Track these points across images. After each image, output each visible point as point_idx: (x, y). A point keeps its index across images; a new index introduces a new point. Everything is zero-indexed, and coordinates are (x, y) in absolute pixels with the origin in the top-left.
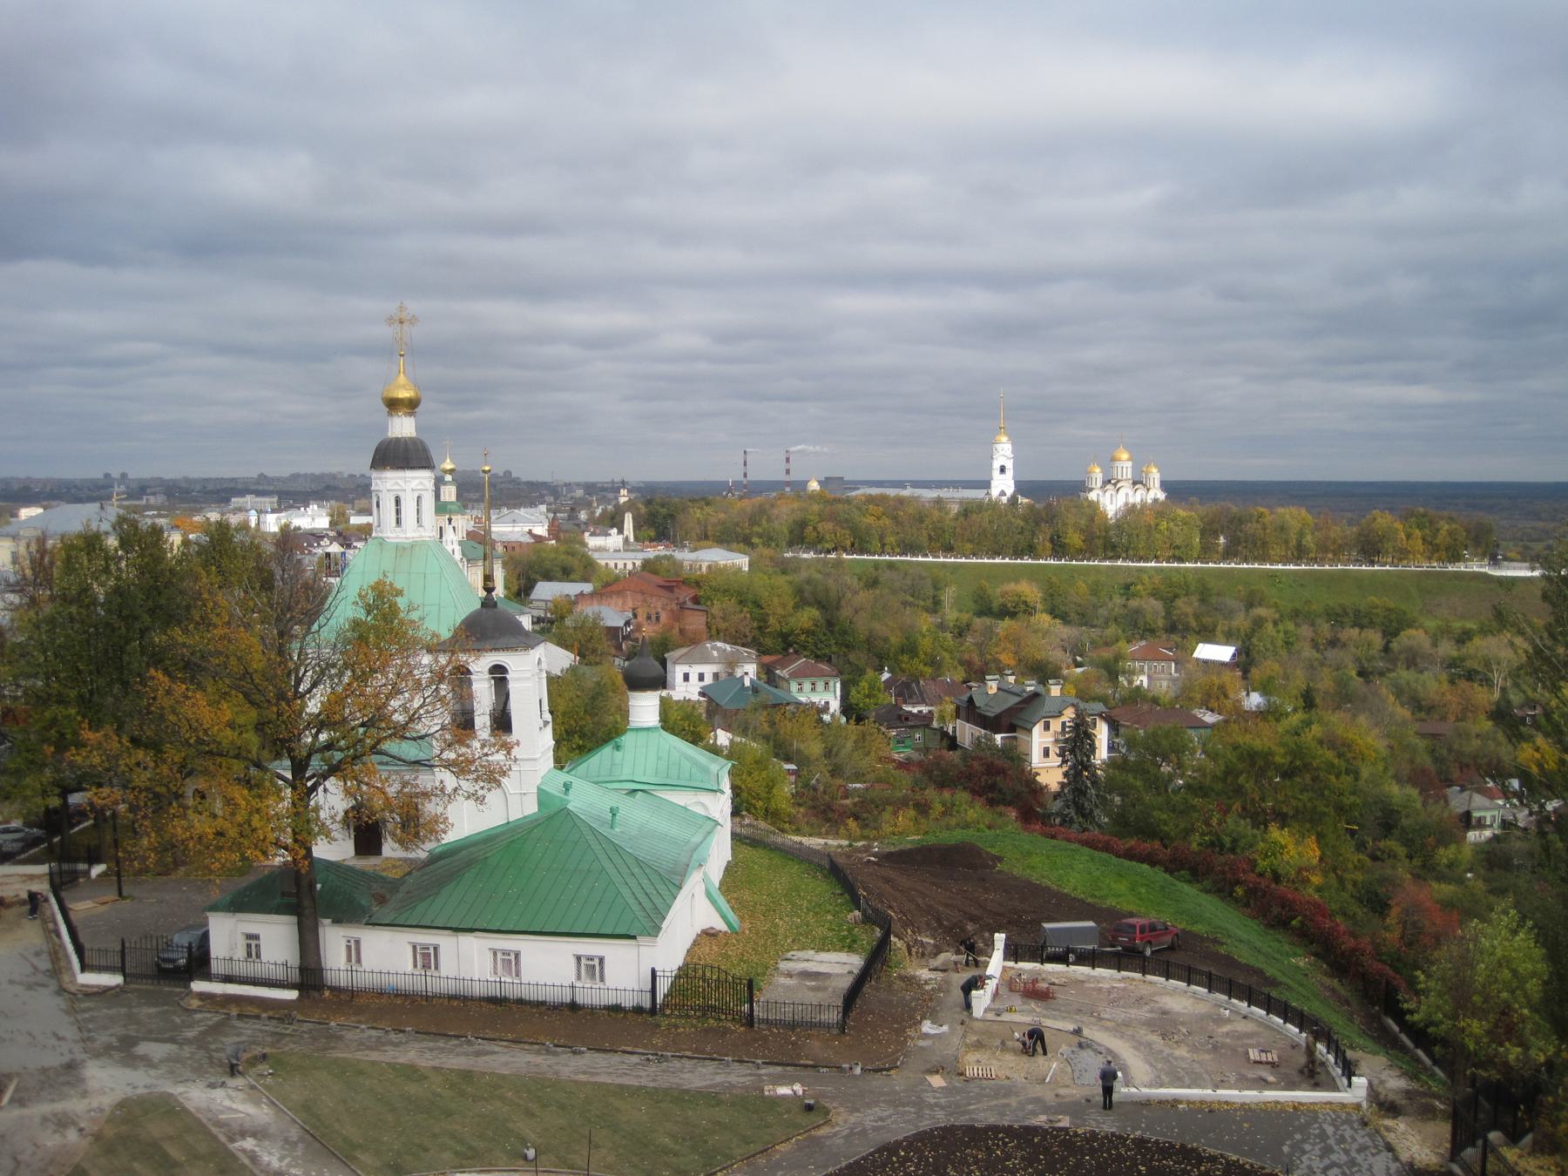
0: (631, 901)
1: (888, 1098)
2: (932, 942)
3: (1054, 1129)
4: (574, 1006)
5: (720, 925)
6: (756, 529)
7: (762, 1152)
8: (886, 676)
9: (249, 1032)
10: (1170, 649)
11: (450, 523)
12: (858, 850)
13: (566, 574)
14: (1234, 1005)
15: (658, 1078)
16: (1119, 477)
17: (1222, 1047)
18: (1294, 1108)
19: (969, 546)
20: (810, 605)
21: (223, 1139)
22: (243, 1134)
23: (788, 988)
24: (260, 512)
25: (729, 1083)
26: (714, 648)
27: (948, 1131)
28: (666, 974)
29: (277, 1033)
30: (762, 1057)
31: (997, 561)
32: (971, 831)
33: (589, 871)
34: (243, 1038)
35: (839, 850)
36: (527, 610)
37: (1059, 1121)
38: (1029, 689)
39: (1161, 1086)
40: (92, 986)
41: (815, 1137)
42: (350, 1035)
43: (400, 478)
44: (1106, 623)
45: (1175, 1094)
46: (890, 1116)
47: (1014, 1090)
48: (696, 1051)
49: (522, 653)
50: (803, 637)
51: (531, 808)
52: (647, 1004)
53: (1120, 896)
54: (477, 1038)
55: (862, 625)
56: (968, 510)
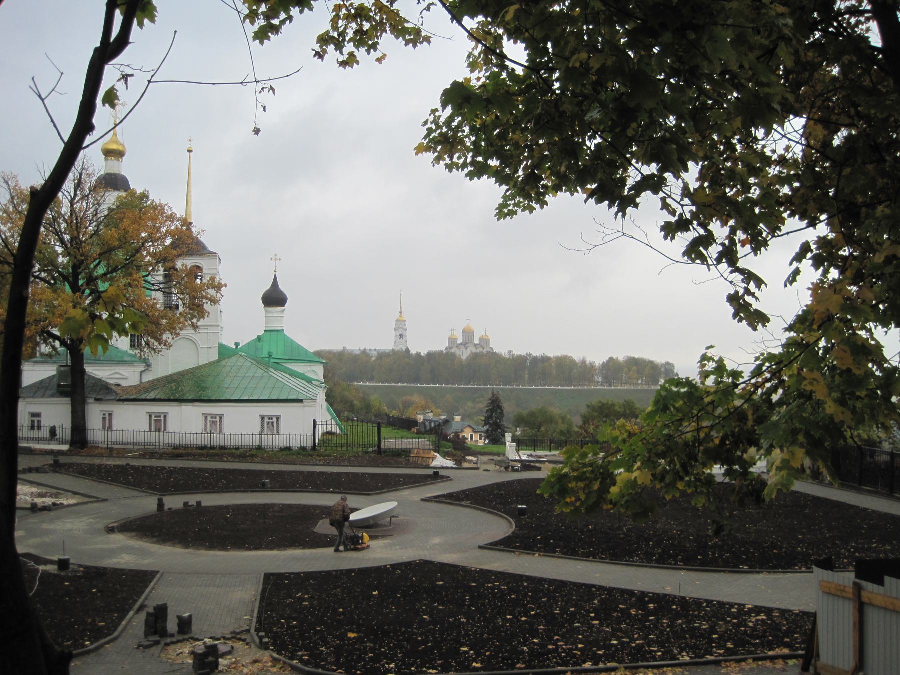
52: (310, 444)
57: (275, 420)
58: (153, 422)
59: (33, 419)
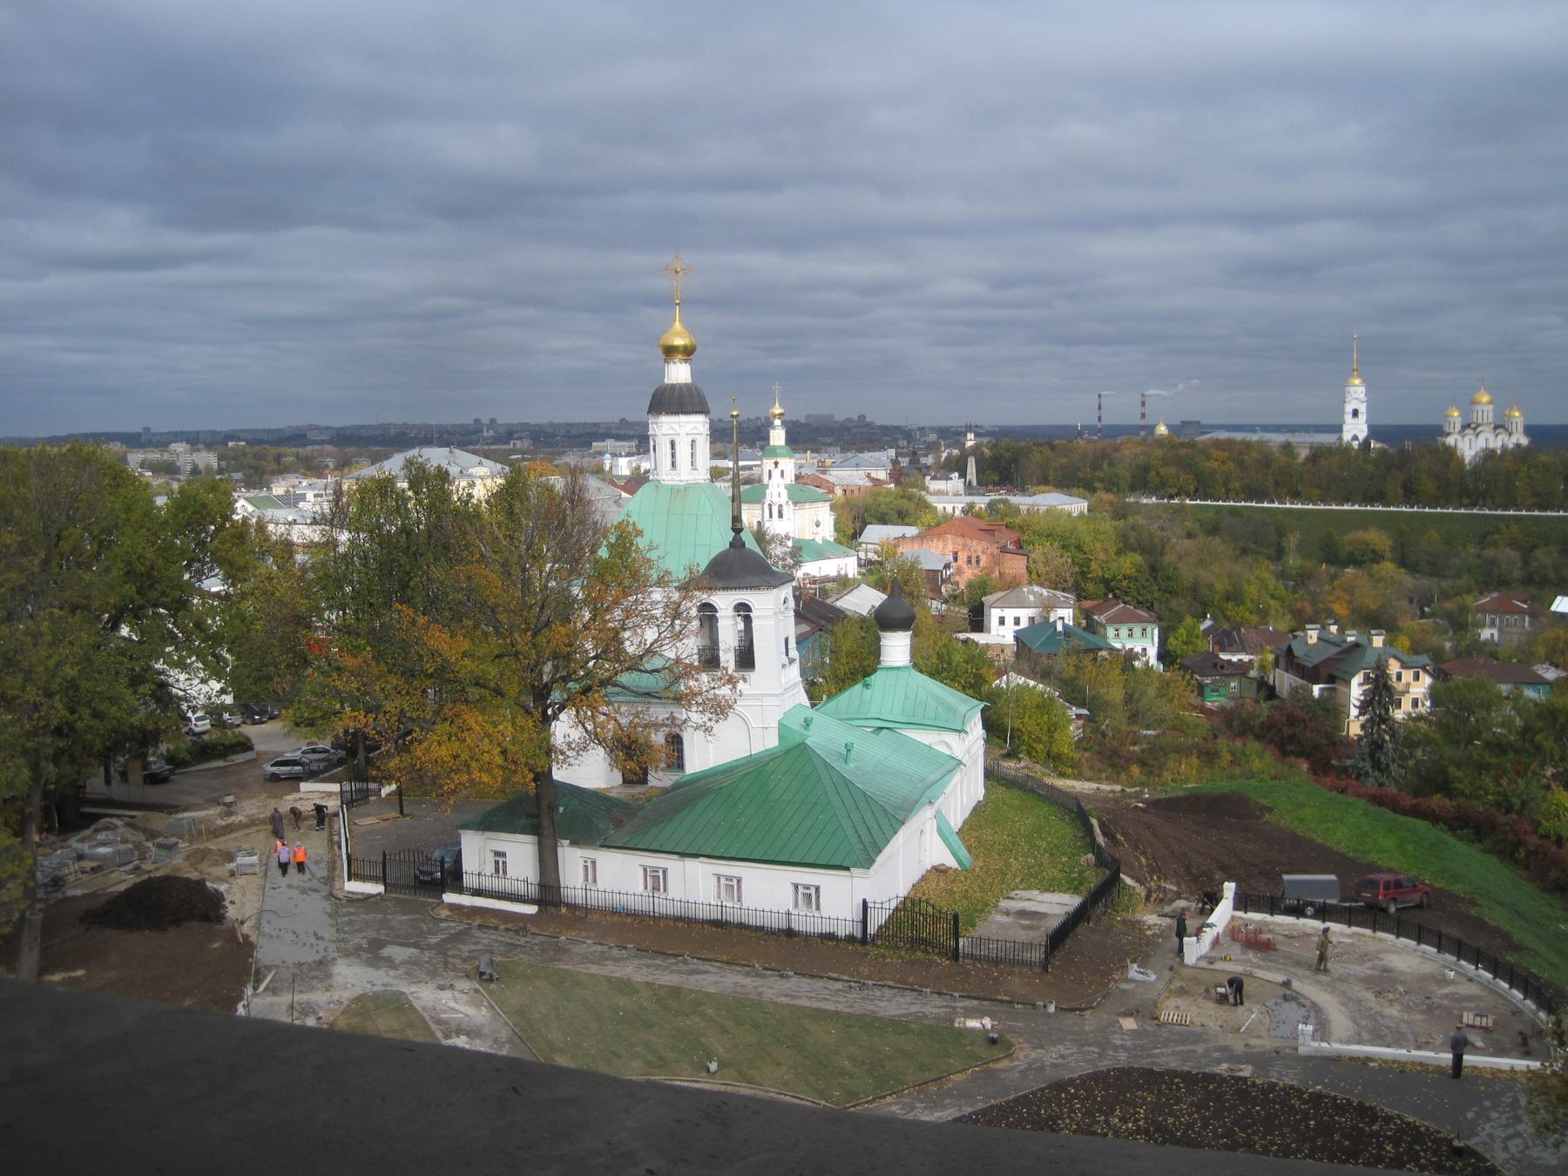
1: (1075, 1037)
2: (1175, 889)
3: (1233, 1077)
4: (790, 933)
5: (951, 863)
6: (1099, 474)
7: (935, 1080)
8: (1208, 623)
9: (486, 941)
10: (1525, 602)
12: (1130, 796)
13: (902, 517)
14: (1461, 967)
15: (856, 1005)
16: (1480, 421)
17: (1436, 1009)
18: (1493, 1074)
19: (1316, 492)
20: (1133, 550)
21: (439, 1035)
22: (458, 1033)
23: (1002, 925)
24: (614, 455)
25: (923, 1013)
27: (1124, 1073)
28: (877, 906)
29: (510, 944)
30: (963, 990)
31: (1346, 507)
32: (1254, 782)
33: (815, 804)
34: (479, 947)
35: (1111, 795)
37: (1241, 1070)
38: (1350, 639)
39: (1359, 1043)
40: (357, 893)
41: (990, 1069)
42: (576, 949)
43: (675, 423)
44: (1459, 576)
45: (1366, 1052)
46: (1072, 1055)
47: (1205, 1037)
48: (899, 981)
49: (765, 591)
50: (1125, 583)
51: (772, 742)
52: (858, 934)
53: (1384, 851)
54: (692, 958)
55: (1187, 572)
56: (1318, 454)
57: (735, 882)
59: (497, 859)
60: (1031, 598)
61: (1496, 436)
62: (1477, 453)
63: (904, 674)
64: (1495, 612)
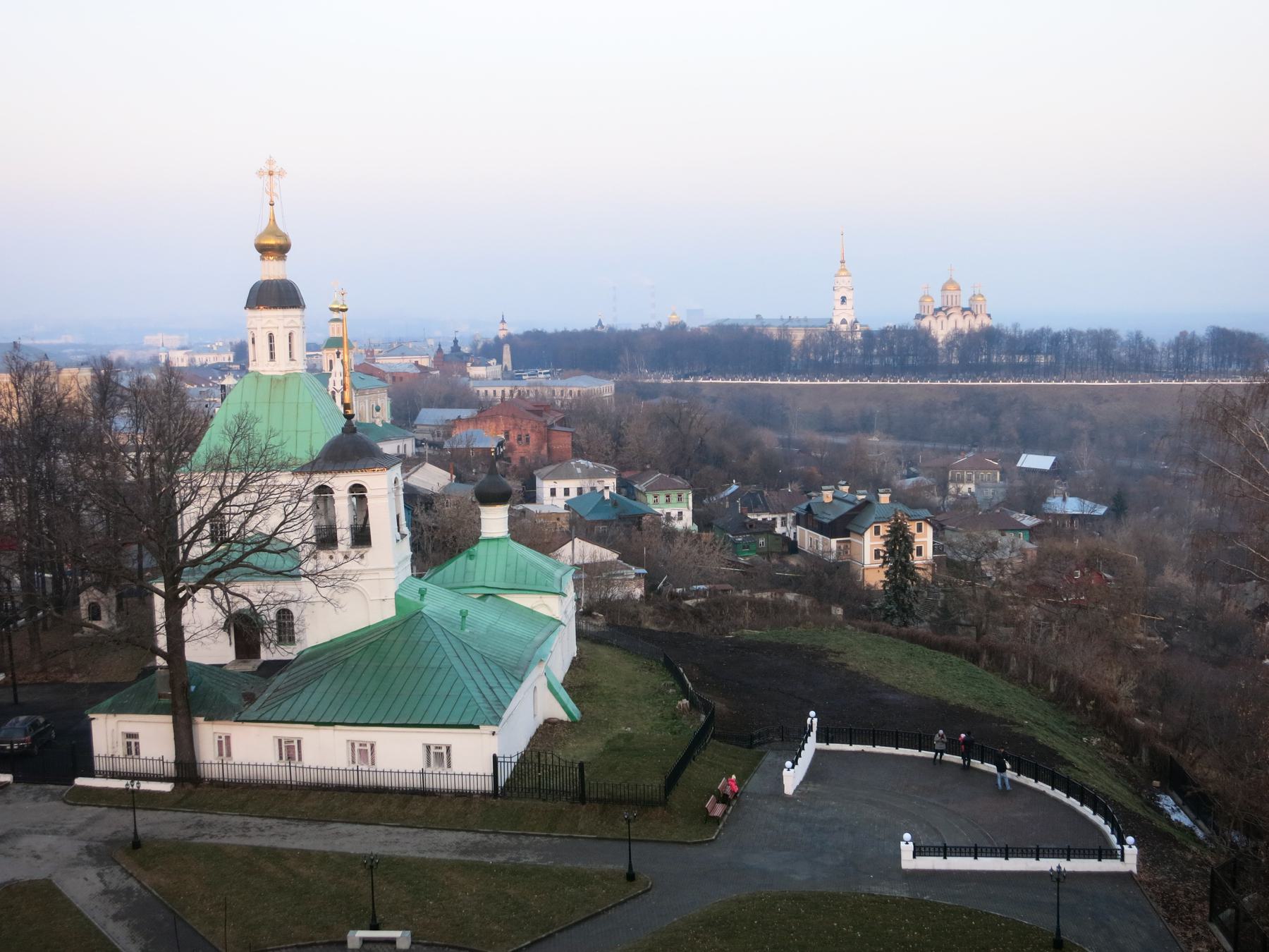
0: (476, 694)
4: (423, 793)
5: (563, 716)
11: (338, 357)
16: (950, 305)
26: (579, 465)
28: (506, 760)
36: (411, 434)
38: (861, 497)
49: (380, 473)
51: (389, 612)
52: (489, 787)
58: (432, 756)
60: (579, 470)
61: (964, 317)
62: (949, 333)
63: (503, 545)
64: (972, 469)
